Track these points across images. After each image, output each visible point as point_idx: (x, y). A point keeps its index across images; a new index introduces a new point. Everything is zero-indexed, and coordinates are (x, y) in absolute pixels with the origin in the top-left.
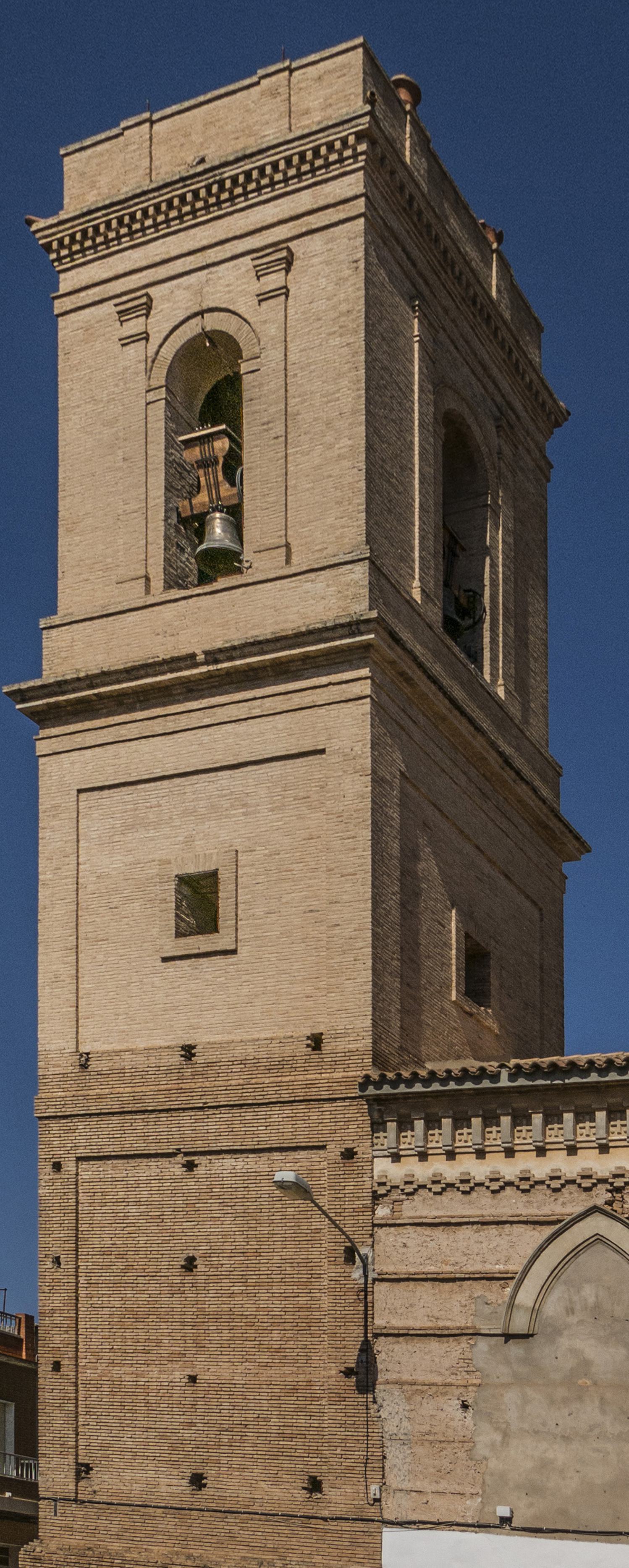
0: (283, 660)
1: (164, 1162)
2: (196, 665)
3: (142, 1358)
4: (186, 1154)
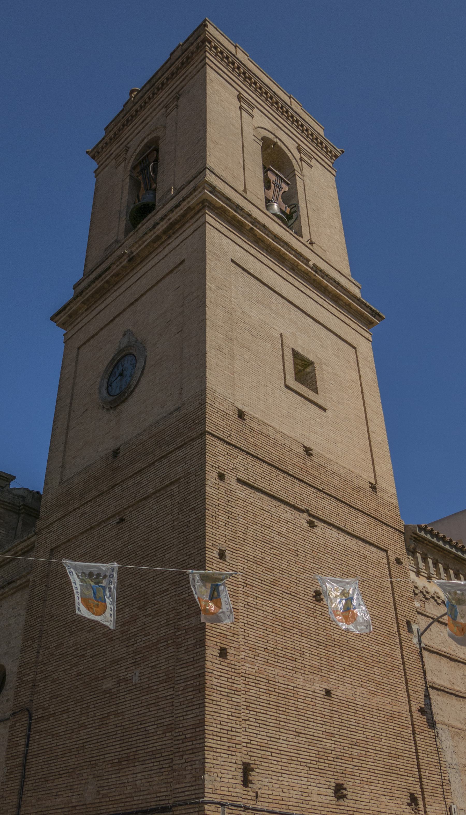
0: (340, 297)
1: (296, 513)
2: (307, 265)
3: (291, 664)
4: (310, 515)
